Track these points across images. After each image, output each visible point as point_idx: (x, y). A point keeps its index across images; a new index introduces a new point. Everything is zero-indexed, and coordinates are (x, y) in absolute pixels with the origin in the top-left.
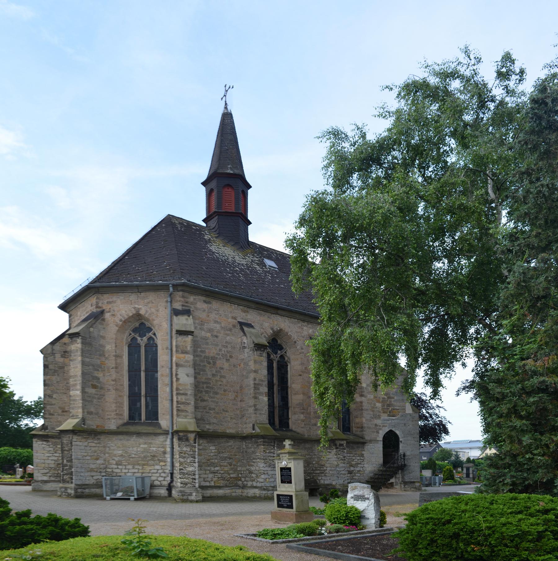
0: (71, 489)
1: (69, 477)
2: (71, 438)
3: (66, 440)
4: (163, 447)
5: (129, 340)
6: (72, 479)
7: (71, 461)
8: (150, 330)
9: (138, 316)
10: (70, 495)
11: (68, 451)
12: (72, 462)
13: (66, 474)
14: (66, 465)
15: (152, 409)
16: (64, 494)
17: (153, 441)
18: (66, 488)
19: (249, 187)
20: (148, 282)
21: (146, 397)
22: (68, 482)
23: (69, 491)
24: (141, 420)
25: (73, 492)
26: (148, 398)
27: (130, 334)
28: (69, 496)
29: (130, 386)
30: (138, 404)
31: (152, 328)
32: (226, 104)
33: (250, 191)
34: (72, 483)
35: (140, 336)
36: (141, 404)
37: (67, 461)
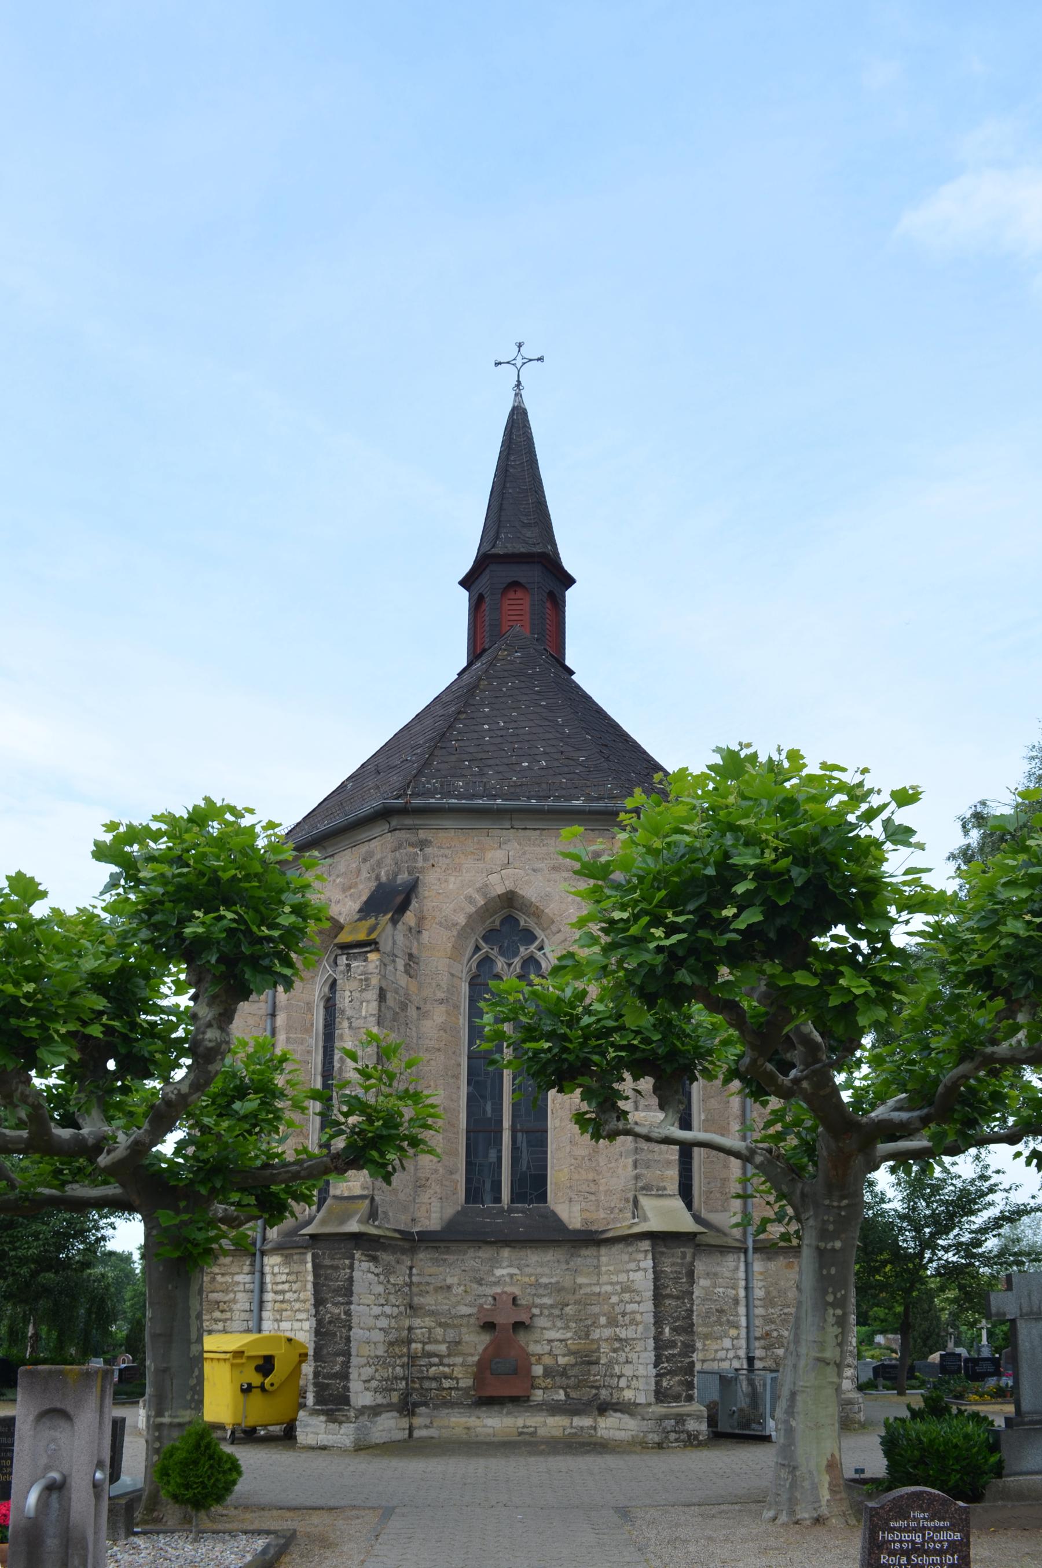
0: (698, 1418)
1: (681, 1383)
2: (688, 1258)
3: (673, 1264)
4: (733, 1288)
5: (474, 965)
6: (690, 1385)
7: (688, 1329)
8: (529, 937)
9: (510, 901)
10: (696, 1437)
11: (677, 1298)
12: (692, 1333)
13: (670, 1372)
14: (672, 1344)
15: (528, 1168)
16: (673, 1436)
17: (718, 1269)
18: (680, 1419)
19: (570, 581)
20: (454, 801)
21: (514, 1131)
22: (677, 1398)
23: (692, 1425)
24: (498, 1199)
25: (704, 1427)
26: (519, 1135)
27: (477, 949)
28: (691, 1441)
29: (470, 1098)
30: (492, 1154)
31: (538, 932)
32: (519, 384)
33: (570, 594)
34: (690, 1398)
35: (502, 953)
36: (500, 1151)
37: (674, 1330)
